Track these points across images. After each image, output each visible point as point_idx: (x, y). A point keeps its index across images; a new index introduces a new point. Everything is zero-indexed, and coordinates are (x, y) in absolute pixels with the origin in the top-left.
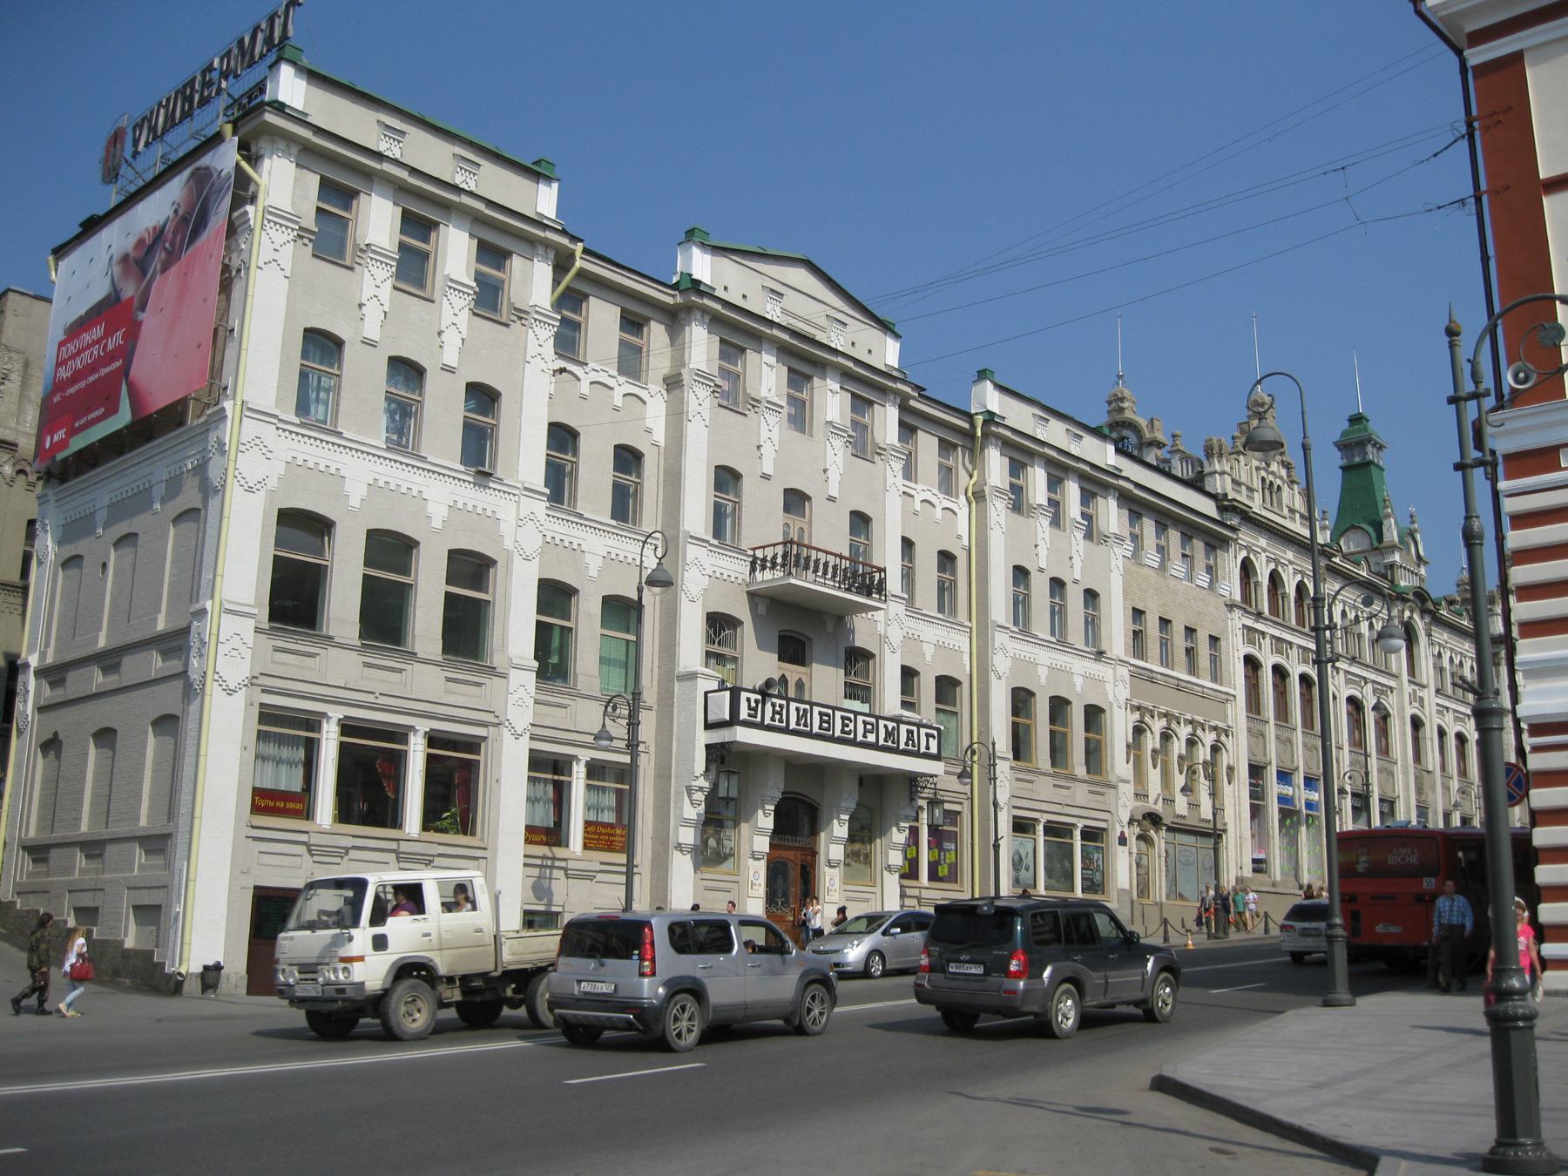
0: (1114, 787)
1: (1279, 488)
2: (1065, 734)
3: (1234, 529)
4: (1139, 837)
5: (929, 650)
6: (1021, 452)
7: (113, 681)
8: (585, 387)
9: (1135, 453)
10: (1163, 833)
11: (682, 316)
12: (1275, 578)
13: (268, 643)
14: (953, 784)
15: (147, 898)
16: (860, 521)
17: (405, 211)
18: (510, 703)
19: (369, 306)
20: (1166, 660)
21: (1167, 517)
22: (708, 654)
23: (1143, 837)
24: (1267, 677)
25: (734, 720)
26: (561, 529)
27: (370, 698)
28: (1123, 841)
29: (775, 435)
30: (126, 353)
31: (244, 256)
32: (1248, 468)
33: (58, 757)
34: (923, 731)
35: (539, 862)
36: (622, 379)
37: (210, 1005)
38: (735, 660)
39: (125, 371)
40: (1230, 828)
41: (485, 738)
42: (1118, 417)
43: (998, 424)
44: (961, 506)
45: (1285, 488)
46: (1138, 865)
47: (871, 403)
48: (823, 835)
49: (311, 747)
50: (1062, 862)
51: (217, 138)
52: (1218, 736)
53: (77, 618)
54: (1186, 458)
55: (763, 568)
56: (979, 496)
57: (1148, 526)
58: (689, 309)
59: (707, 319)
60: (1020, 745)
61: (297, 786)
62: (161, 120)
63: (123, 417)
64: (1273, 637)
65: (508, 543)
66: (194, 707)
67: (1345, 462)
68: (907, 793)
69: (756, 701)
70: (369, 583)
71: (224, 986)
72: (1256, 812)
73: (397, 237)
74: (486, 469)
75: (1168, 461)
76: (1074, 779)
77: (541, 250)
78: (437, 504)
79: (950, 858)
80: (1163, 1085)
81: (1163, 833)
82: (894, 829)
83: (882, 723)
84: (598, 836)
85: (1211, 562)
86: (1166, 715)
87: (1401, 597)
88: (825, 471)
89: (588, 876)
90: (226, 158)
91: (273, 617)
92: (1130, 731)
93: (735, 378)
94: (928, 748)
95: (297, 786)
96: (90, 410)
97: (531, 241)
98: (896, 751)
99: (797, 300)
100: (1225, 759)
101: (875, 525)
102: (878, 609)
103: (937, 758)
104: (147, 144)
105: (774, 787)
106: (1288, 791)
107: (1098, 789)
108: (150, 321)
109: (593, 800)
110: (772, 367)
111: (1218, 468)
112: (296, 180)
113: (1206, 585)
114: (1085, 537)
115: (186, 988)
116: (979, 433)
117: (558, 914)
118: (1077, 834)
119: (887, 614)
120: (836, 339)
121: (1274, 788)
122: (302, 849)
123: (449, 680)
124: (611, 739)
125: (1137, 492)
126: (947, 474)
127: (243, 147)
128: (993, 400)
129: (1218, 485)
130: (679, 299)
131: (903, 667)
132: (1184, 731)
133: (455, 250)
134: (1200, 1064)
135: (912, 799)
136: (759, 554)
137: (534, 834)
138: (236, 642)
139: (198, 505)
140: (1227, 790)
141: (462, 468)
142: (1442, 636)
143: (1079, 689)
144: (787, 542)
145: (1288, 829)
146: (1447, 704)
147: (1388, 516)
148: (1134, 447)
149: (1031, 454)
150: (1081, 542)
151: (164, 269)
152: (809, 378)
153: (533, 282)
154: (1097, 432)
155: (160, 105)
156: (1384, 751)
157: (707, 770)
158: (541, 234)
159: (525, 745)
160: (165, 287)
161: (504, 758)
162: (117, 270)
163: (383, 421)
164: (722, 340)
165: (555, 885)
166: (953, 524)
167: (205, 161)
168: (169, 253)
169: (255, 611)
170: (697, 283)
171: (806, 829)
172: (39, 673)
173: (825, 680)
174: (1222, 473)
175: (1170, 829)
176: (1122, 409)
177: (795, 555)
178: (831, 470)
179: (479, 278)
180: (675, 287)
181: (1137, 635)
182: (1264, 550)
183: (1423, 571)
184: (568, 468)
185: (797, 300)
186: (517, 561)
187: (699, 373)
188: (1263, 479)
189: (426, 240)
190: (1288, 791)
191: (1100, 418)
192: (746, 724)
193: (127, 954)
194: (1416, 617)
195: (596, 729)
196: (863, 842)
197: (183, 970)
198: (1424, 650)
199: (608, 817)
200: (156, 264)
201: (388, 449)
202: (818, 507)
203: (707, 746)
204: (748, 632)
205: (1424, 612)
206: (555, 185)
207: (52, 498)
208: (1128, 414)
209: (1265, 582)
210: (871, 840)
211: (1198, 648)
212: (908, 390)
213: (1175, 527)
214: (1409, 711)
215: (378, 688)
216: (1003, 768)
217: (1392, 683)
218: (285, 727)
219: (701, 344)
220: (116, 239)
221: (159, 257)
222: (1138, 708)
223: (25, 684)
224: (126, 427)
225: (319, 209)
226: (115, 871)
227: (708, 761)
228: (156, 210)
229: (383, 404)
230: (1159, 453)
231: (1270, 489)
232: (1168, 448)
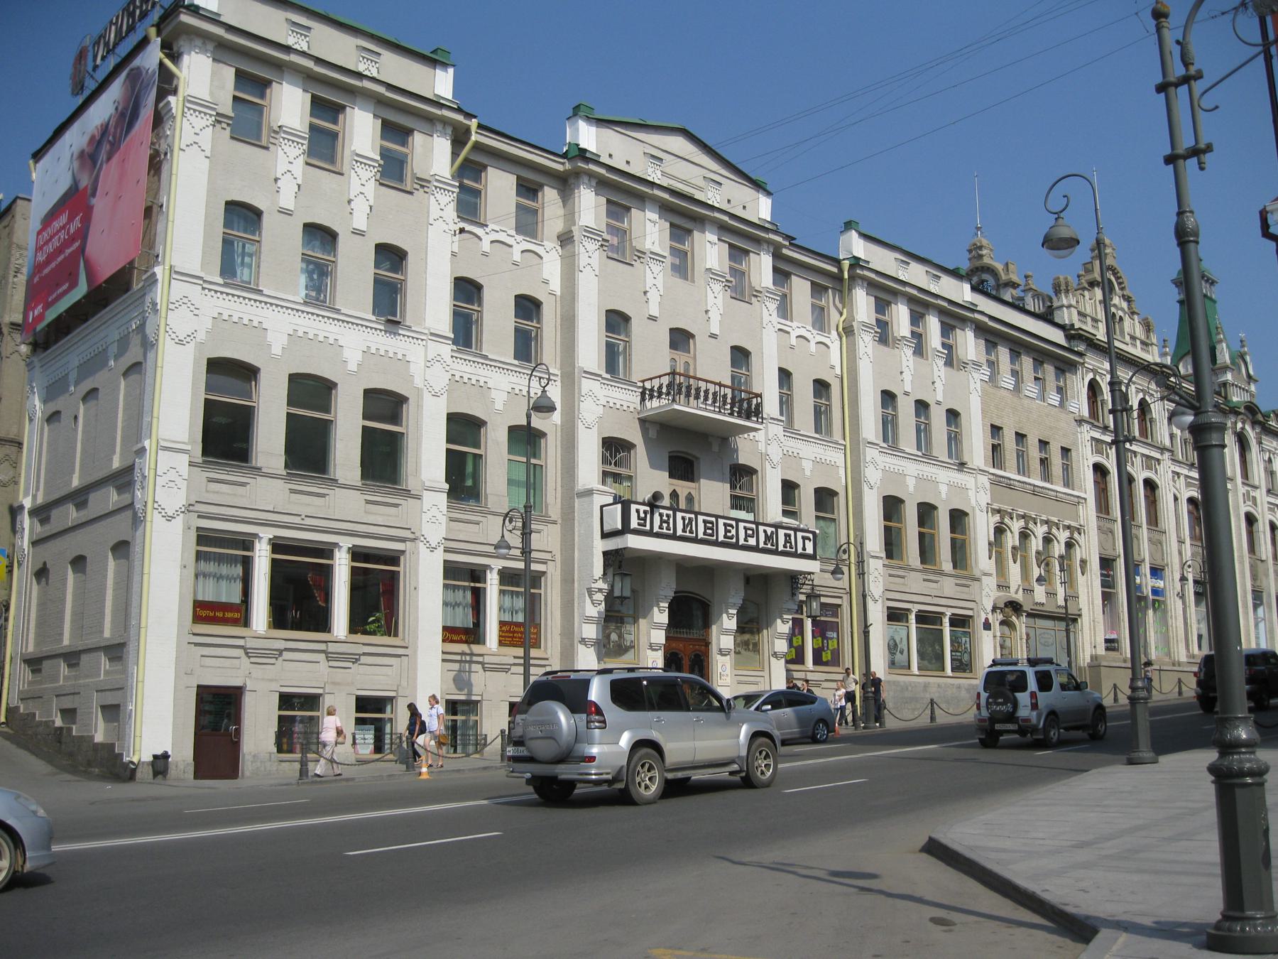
0: (978, 580)
2: (932, 536)
3: (1080, 354)
4: (1002, 623)
5: (807, 466)
6: (885, 291)
8: (486, 245)
9: (994, 293)
10: (1024, 619)
11: (571, 181)
13: (202, 475)
14: (828, 580)
15: (110, 699)
16: (740, 355)
17: (314, 98)
18: (424, 520)
19: (284, 180)
20: (1022, 469)
21: (1019, 345)
22: (605, 474)
25: (626, 529)
26: (466, 368)
27: (297, 520)
28: (987, 626)
30: (82, 234)
31: (169, 140)
32: (1092, 301)
34: (800, 535)
35: (458, 658)
36: (520, 238)
37: (158, 789)
38: (630, 478)
39: (82, 249)
40: (1085, 612)
41: (403, 552)
42: (978, 264)
43: (863, 268)
44: (833, 340)
45: (1127, 318)
46: (1002, 647)
47: (747, 252)
48: (714, 628)
49: (247, 563)
50: (932, 646)
51: (145, 42)
52: (1072, 534)
53: (59, 462)
54: (1037, 295)
55: (651, 397)
56: (848, 331)
57: (1003, 353)
58: (577, 174)
59: (594, 183)
60: (892, 545)
61: (236, 598)
62: (112, 36)
63: (82, 290)
64: (1143, 455)
65: (418, 382)
66: (139, 533)
69: (645, 512)
70: (292, 421)
71: (172, 772)
72: (1108, 598)
73: (308, 119)
74: (398, 319)
75: (1022, 299)
76: (942, 573)
77: (439, 127)
78: (352, 351)
80: (935, 849)
81: (1024, 619)
82: (779, 621)
83: (761, 528)
84: (510, 634)
85: (1062, 384)
86: (1023, 517)
87: (1234, 411)
88: (707, 312)
90: (153, 56)
91: (205, 452)
92: (992, 531)
93: (622, 234)
94: (804, 549)
95: (236, 598)
96: (58, 286)
97: (430, 120)
98: (775, 552)
99: (676, 164)
100: (1078, 554)
101: (754, 359)
102: (756, 430)
103: (813, 557)
104: (103, 58)
105: (667, 587)
107: (901, 573)
108: (100, 204)
109: (450, 598)
110: (655, 223)
111: (1065, 302)
112: (213, 74)
113: (1057, 404)
114: (945, 364)
115: (139, 775)
116: (846, 276)
117: (478, 702)
118: (946, 621)
119: (767, 434)
120: (713, 197)
122: (240, 652)
123: (368, 502)
124: (509, 548)
125: (991, 324)
127: (167, 47)
128: (857, 247)
129: (1065, 317)
130: (568, 166)
131: (783, 481)
132: (1040, 530)
133: (361, 130)
134: (969, 831)
135: (793, 594)
136: (648, 385)
137: (450, 633)
139: (140, 359)
140: (1081, 580)
141: (374, 318)
143: (944, 496)
144: (673, 373)
147: (1221, 341)
148: (993, 288)
149: (895, 293)
150: (943, 368)
151: (109, 159)
152: (689, 232)
153: (434, 155)
154: (955, 273)
155: (111, 23)
157: (605, 574)
159: (439, 558)
160: (109, 173)
161: (421, 568)
162: (76, 164)
163: (303, 280)
164: (608, 201)
165: (474, 677)
166: (828, 356)
167: (137, 62)
168: (112, 144)
169: (189, 447)
171: (700, 623)
172: (32, 513)
173: (713, 494)
174: (1069, 307)
175: (1029, 615)
176: (981, 256)
177: (679, 385)
178: (711, 312)
179: (384, 153)
180: (565, 156)
181: (995, 448)
183: (1253, 388)
184: (474, 318)
185: (676, 164)
187: (587, 230)
189: (335, 122)
191: (965, 266)
193: (97, 747)
194: (1248, 427)
195: (496, 539)
196: (752, 633)
197: (135, 760)
199: (520, 618)
200: (103, 155)
201: (306, 303)
202: (701, 344)
203: (605, 553)
204: (640, 455)
205: (1254, 423)
206: (451, 70)
207: (37, 364)
208: (986, 260)
210: (759, 631)
211: (1051, 458)
212: (779, 239)
213: (1028, 354)
214: (1244, 509)
215: (305, 511)
216: (876, 567)
218: (218, 547)
219: (589, 205)
220: (75, 139)
221: (106, 147)
223: (22, 523)
224: (84, 297)
225: (235, 98)
226: (87, 676)
227: (606, 566)
228: (102, 110)
229: (299, 265)
232: (1022, 288)
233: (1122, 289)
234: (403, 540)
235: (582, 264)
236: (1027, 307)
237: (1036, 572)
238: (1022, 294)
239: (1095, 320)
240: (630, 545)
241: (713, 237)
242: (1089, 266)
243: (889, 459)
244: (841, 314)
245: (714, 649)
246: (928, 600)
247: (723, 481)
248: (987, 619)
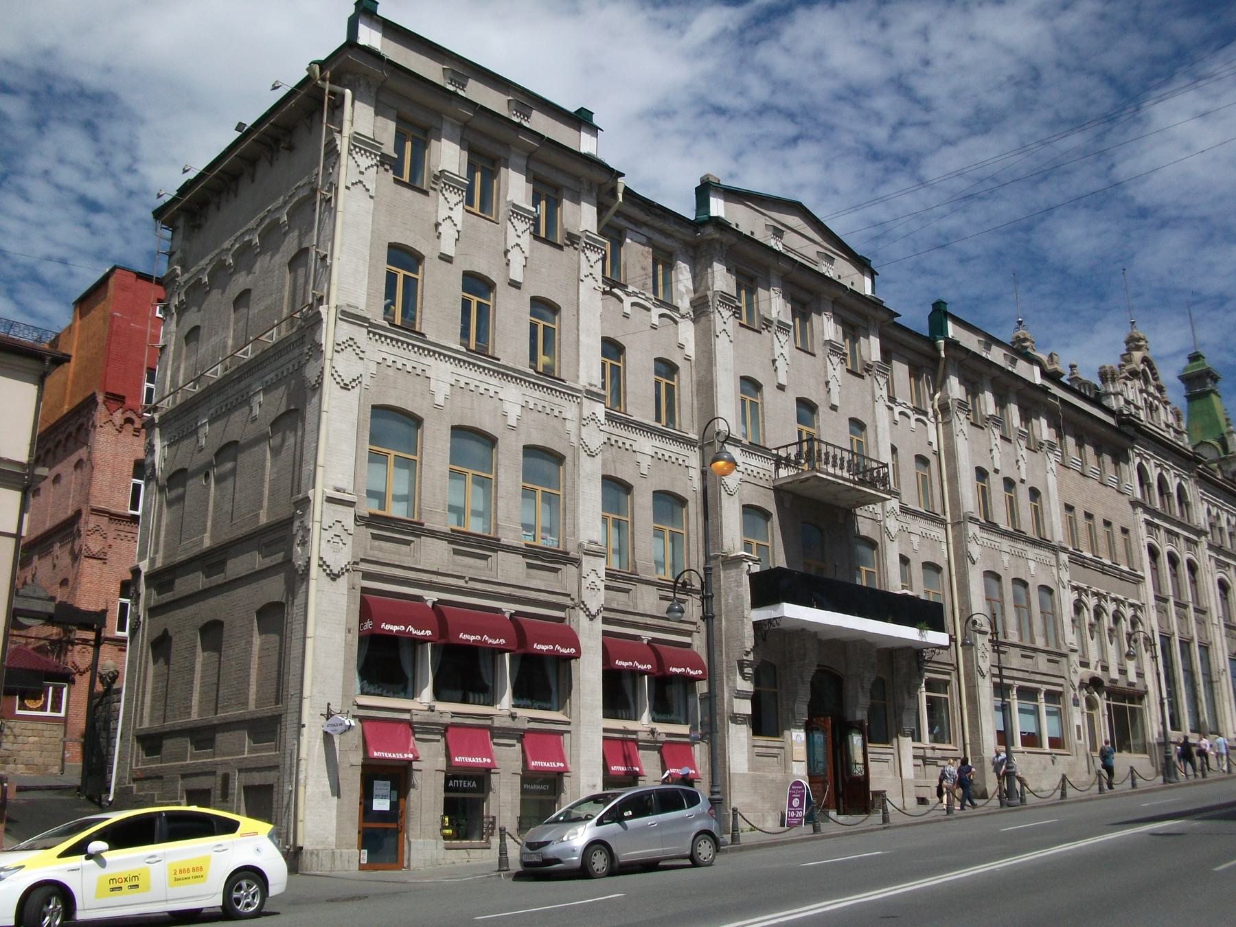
1: (1157, 408)
7: (218, 579)
8: (627, 308)
15: (257, 779)
24: (1164, 561)
27: (461, 583)
28: (1076, 702)
29: (786, 351)
32: (1132, 390)
33: (167, 662)
129: (1114, 403)
136: (782, 453)
144: (800, 443)
172: (149, 577)
177: (809, 448)
226: (224, 754)
233: (1156, 379)
234: (562, 607)
239: (1137, 408)
246: (1026, 676)
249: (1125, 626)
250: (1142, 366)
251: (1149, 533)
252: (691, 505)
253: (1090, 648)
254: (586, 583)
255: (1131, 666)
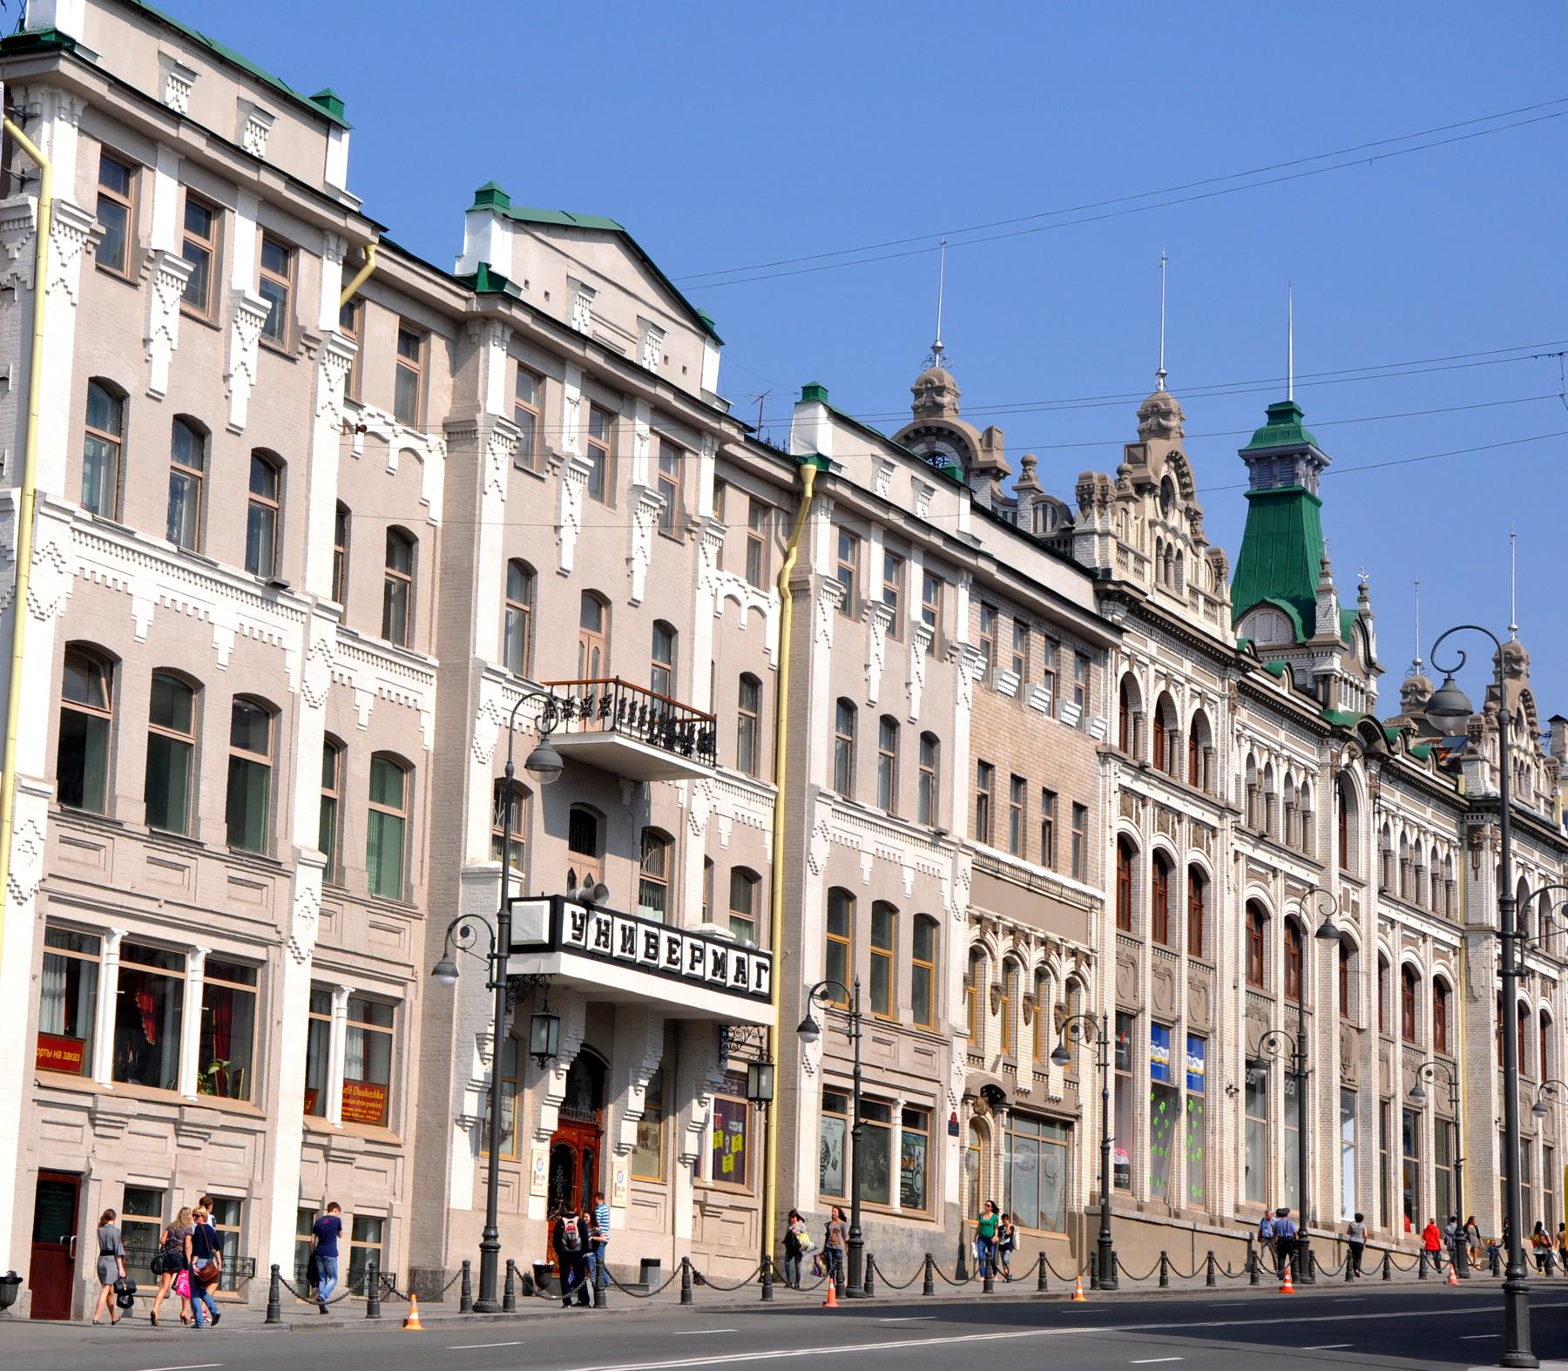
1: (1180, 555)
11: (475, 329)
12: (1165, 706)
20: (1017, 847)
23: (978, 1125)
24: (1277, 936)
25: (554, 945)
27: (152, 907)
28: (954, 1129)
36: (399, 428)
40: (1086, 1112)
41: (262, 962)
42: (932, 421)
44: (770, 601)
45: (1188, 554)
56: (799, 590)
58: (486, 319)
64: (1157, 804)
67: (1255, 490)
68: (716, 1048)
76: (898, 1029)
78: (214, 624)
79: (736, 1144)
81: (1004, 1118)
82: (695, 1102)
87: (1339, 734)
89: (347, 1158)
94: (759, 985)
101: (292, 475)
105: (570, 1039)
106: (1162, 1055)
107: (925, 1046)
111: (1098, 526)
116: (809, 493)
118: (897, 1114)
121: (1147, 1052)
123: (232, 880)
125: (1001, 577)
126: (409, 386)
128: (828, 438)
129: (1096, 553)
130: (476, 306)
135: (722, 1058)
136: (561, 693)
138: (29, 833)
142: (1393, 796)
145: (1163, 1117)
146: (1393, 914)
156: (1296, 990)
158: (651, 389)
170: (498, 281)
174: (1105, 534)
176: (939, 407)
178: (640, 566)
180: (467, 282)
182: (1153, 661)
183: (1373, 685)
186: (304, 705)
187: (59, 206)
188: (1159, 541)
190: (1162, 1055)
192: (570, 949)
198: (1365, 820)
205: (1369, 755)
206: (346, 137)
208: (949, 417)
209: (1152, 714)
211: (1052, 821)
217: (1313, 879)
222: (978, 920)
230: (995, 485)
231: (1168, 556)
235: (488, 480)
236: (1021, 525)
237: (1054, 1042)
238: (1014, 496)
239: (1140, 559)
240: (563, 971)
241: (573, 391)
242: (1139, 452)
243: (842, 823)
244: (786, 556)
245: (609, 1141)
247: (632, 858)
248: (954, 1115)
249: (1056, 992)
250: (1164, 470)
251: (1125, 812)
252: (419, 772)
253: (988, 1029)
254: (298, 907)
255: (1056, 1073)
